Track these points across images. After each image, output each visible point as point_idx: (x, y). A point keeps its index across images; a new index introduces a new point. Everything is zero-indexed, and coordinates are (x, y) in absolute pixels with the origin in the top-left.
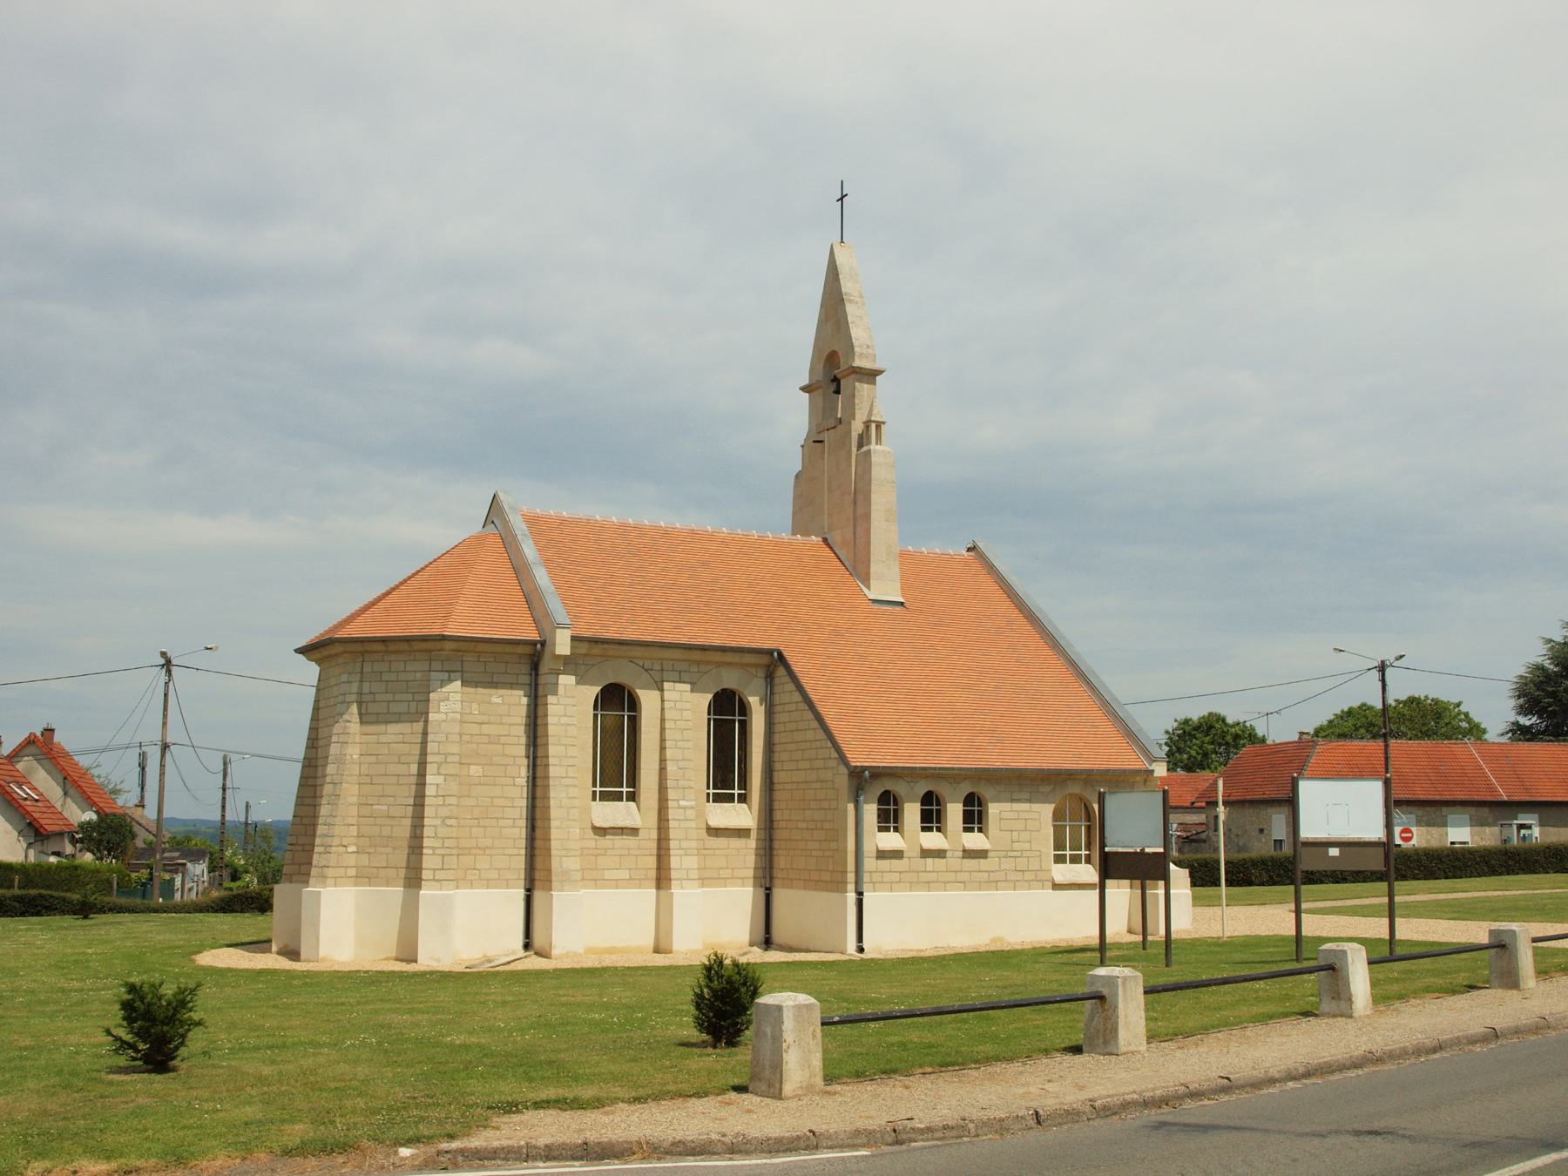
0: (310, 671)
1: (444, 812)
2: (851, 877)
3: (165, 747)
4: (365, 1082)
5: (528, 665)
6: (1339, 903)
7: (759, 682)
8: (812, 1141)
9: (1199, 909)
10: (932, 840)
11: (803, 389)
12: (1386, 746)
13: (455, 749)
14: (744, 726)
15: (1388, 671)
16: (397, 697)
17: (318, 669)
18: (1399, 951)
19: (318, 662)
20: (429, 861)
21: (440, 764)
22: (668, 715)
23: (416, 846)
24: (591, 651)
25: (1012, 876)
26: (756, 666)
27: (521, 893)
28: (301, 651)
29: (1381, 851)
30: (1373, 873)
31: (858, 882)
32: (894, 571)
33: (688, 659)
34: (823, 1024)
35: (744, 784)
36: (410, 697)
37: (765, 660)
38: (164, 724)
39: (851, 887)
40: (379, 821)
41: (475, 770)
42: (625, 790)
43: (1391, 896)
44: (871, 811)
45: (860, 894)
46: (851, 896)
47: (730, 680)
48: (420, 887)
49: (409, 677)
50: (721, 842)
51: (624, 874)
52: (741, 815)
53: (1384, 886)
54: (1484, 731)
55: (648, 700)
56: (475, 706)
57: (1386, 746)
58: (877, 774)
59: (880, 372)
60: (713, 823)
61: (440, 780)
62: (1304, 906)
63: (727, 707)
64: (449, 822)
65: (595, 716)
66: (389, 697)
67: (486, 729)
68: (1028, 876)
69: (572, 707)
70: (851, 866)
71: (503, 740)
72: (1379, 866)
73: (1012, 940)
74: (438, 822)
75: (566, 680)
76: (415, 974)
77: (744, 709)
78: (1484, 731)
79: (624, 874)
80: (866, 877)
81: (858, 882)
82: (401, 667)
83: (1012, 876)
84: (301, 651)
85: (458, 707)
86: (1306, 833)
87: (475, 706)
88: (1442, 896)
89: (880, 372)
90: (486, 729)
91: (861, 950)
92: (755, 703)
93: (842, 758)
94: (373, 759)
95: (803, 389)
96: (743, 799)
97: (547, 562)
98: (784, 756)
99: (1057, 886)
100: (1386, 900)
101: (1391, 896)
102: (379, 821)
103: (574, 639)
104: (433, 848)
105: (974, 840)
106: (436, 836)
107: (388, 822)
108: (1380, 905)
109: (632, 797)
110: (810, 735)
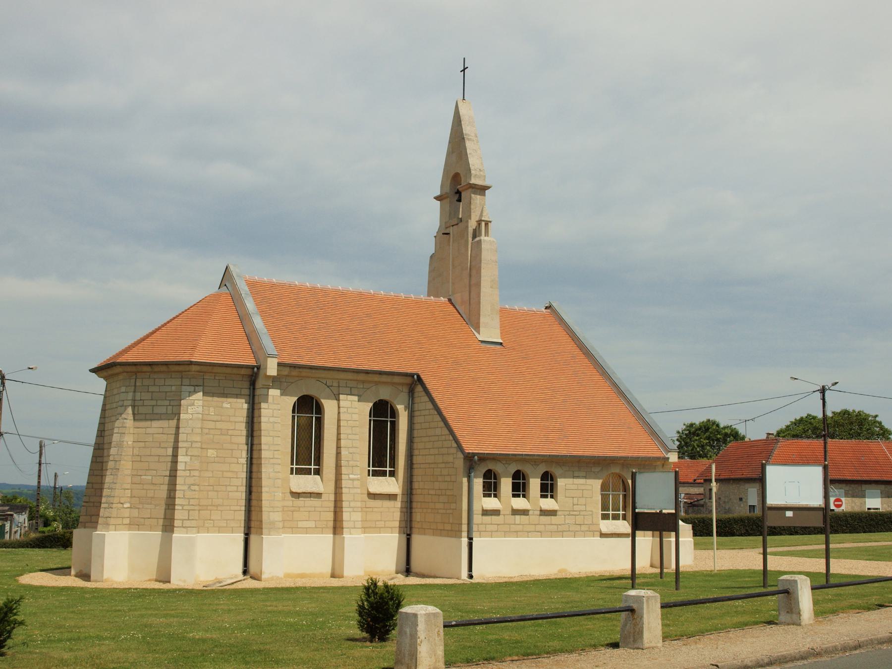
0: (100, 384)
1: (190, 481)
2: (465, 527)
5: (249, 382)
6: (793, 548)
7: (404, 396)
10: (520, 503)
11: (437, 198)
13: (198, 438)
14: (394, 425)
15: (827, 393)
16: (159, 403)
19: (105, 378)
20: (179, 514)
21: (187, 448)
24: (291, 372)
25: (573, 528)
27: (241, 536)
29: (821, 513)
30: (815, 528)
33: (356, 379)
35: (393, 464)
36: (167, 403)
37: (408, 380)
39: (465, 534)
43: (827, 543)
44: (478, 483)
45: (471, 539)
46: (465, 541)
47: (384, 394)
48: (173, 531)
49: (167, 389)
50: (378, 503)
51: (311, 524)
52: (391, 485)
55: (329, 406)
56: (212, 409)
57: (825, 443)
58: (483, 458)
59: (488, 188)
61: (187, 459)
62: (769, 550)
63: (382, 413)
64: (193, 488)
65: (293, 417)
66: (153, 403)
68: (584, 528)
69: (278, 410)
71: (230, 432)
74: (186, 488)
75: (274, 393)
77: (394, 414)
79: (311, 524)
80: (475, 528)
81: (469, 531)
82: (162, 382)
84: (93, 371)
85: (200, 409)
87: (212, 409)
89: (488, 188)
91: (471, 577)
92: (401, 408)
95: (437, 198)
96: (392, 474)
97: (262, 313)
99: (603, 535)
100: (824, 546)
101: (827, 543)
105: (548, 503)
106: (184, 497)
108: (819, 550)
109: (318, 472)
110: (438, 431)
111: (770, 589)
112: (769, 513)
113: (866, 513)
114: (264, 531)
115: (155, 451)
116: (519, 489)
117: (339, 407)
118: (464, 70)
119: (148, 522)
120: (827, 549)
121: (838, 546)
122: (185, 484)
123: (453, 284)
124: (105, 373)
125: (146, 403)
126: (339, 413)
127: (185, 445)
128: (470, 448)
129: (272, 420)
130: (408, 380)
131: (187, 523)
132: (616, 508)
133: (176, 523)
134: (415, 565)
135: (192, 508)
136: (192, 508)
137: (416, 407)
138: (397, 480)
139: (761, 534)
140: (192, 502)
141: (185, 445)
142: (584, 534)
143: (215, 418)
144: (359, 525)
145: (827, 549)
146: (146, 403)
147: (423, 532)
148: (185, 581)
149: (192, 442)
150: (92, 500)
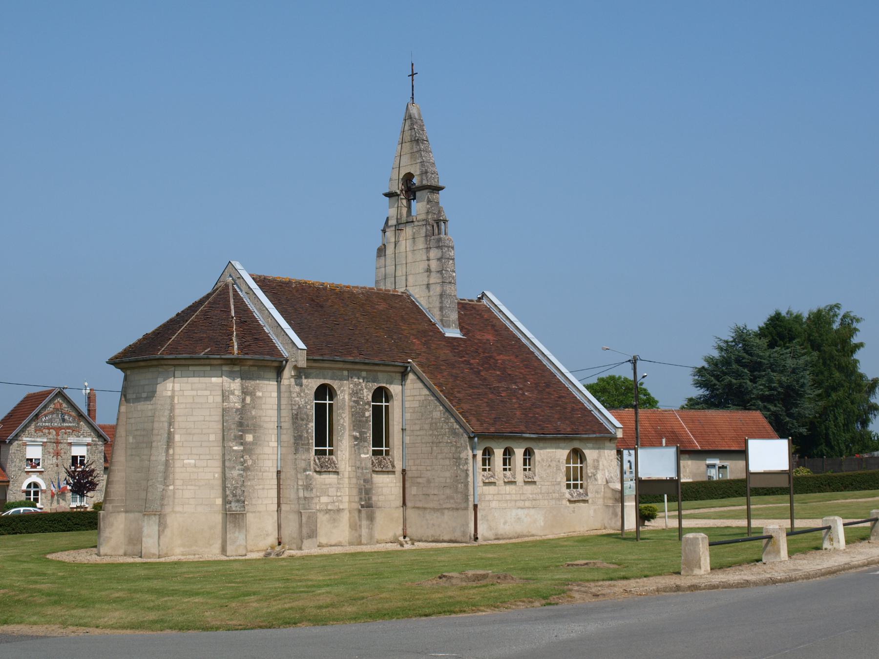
0: (119, 375)
6: (697, 511)
8: (746, 584)
12: (636, 413)
15: (638, 363)
17: (123, 374)
18: (795, 530)
19: (122, 369)
26: (396, 372)
29: (787, 476)
30: (781, 489)
34: (710, 545)
36: (208, 393)
43: (748, 505)
53: (787, 497)
54: (656, 402)
57: (636, 413)
59: (442, 188)
62: (683, 512)
66: (194, 393)
72: (785, 484)
76: (246, 560)
78: (656, 402)
86: (753, 468)
88: (725, 509)
89: (442, 188)
101: (748, 505)
107: (195, 470)
111: (753, 536)
112: (751, 476)
113: (68, 513)
118: (412, 75)
120: (748, 509)
121: (740, 507)
125: (186, 393)
132: (576, 479)
139: (678, 501)
145: (748, 509)
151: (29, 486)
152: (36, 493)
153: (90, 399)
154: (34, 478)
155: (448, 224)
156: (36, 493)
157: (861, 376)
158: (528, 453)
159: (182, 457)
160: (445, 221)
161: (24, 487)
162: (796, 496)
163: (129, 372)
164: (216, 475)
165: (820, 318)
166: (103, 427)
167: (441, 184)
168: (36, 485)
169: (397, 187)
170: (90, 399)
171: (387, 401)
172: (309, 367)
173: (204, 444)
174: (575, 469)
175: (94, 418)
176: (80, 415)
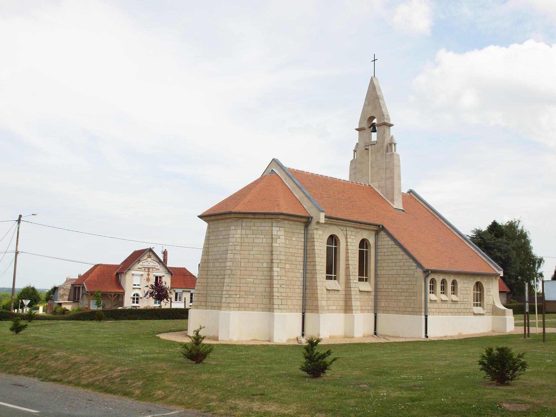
0: (204, 225)
1: (281, 282)
2: (423, 310)
3: (17, 253)
4: (294, 389)
9: (216, 335)
10: (443, 297)
11: (357, 129)
13: (283, 258)
16: (258, 236)
20: (276, 301)
21: (278, 263)
22: (349, 247)
23: (271, 296)
25: (464, 311)
27: (300, 315)
28: (201, 217)
31: (426, 311)
32: (400, 199)
36: (263, 236)
37: (376, 228)
38: (17, 244)
39: (423, 313)
40: (249, 285)
41: (287, 266)
42: (333, 275)
43: (544, 320)
45: (426, 316)
46: (424, 317)
48: (273, 312)
49: (262, 228)
51: (334, 308)
52: (367, 286)
56: (287, 241)
60: (361, 289)
61: (279, 269)
64: (283, 286)
66: (254, 236)
67: (291, 250)
68: (468, 311)
70: (423, 306)
71: (296, 255)
73: (464, 333)
74: (279, 286)
79: (334, 308)
80: (429, 310)
81: (426, 311)
82: (259, 224)
83: (464, 311)
84: (201, 217)
85: (283, 241)
87: (287, 241)
89: (392, 125)
90: (291, 250)
91: (427, 337)
93: (419, 265)
94: (247, 260)
95: (357, 129)
98: (265, 265)
99: (475, 314)
100: (542, 320)
101: (544, 320)
102: (249, 285)
103: (326, 217)
104: (278, 296)
105: (454, 297)
106: (278, 292)
107: (253, 285)
108: (521, 323)
110: (400, 257)
114: (320, 311)
115: (255, 265)
116: (443, 289)
117: (347, 242)
119: (251, 306)
120: (544, 322)
122: (278, 284)
123: (372, 177)
124: (209, 218)
126: (347, 245)
127: (277, 261)
128: (427, 267)
129: (320, 248)
130: (376, 228)
131: (281, 307)
133: (275, 307)
134: (378, 331)
135: (283, 298)
136: (283, 298)
137: (379, 243)
138: (370, 284)
140: (283, 294)
141: (277, 261)
142: (464, 314)
143: (289, 246)
144: (359, 308)
145: (544, 322)
146: (249, 236)
147: (433, 313)
148: (281, 340)
149: (280, 260)
150: (201, 293)
151: (134, 295)
152: (137, 299)
153: (165, 253)
154: (137, 291)
155: (397, 145)
156: (137, 299)
157: (533, 256)
158: (454, 283)
159: (245, 277)
160: (395, 144)
161: (132, 296)
162: (530, 315)
163: (211, 223)
164: (267, 290)
165: (512, 226)
166: (171, 268)
167: (391, 123)
168: (137, 295)
169: (365, 125)
170: (165, 253)
171: (367, 248)
172: (325, 223)
173: (260, 269)
174: (477, 294)
175: (166, 263)
176: (160, 261)
